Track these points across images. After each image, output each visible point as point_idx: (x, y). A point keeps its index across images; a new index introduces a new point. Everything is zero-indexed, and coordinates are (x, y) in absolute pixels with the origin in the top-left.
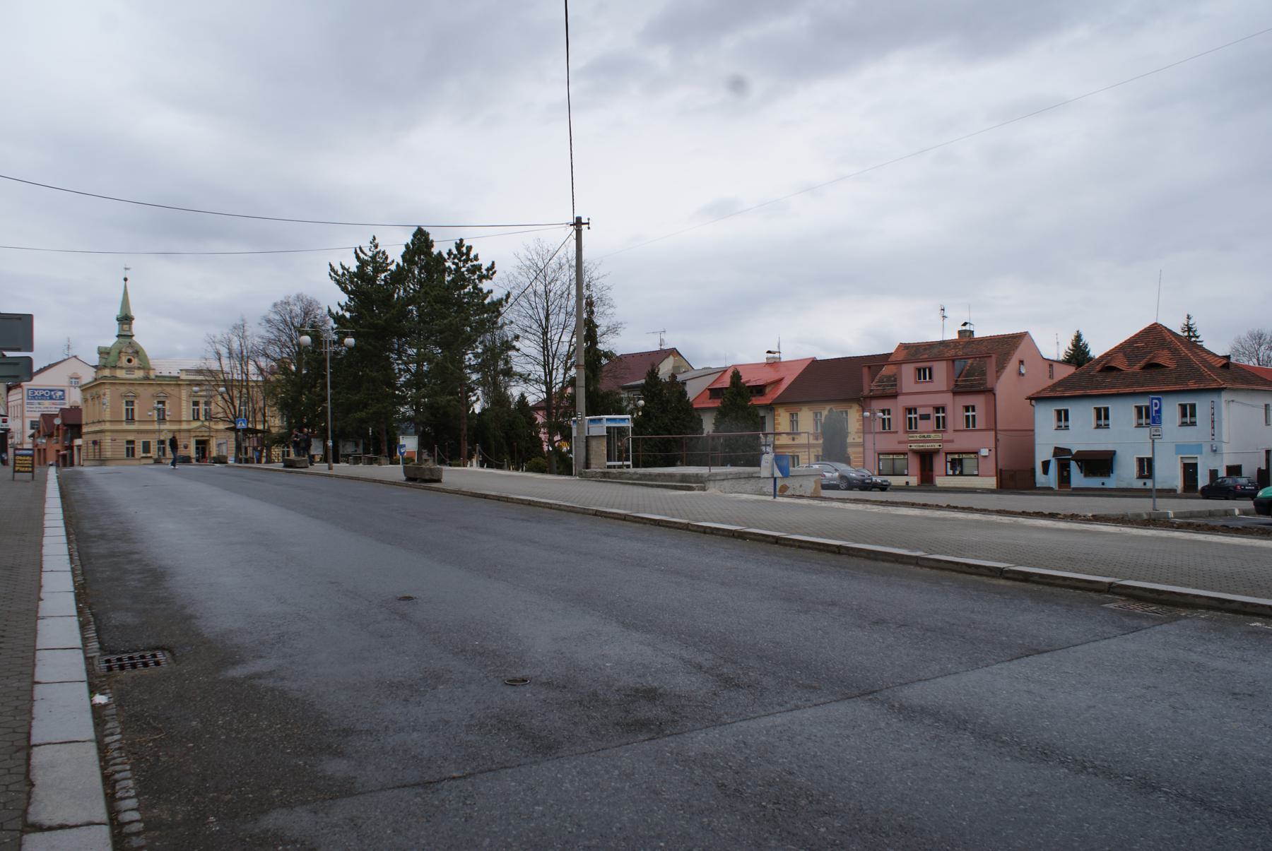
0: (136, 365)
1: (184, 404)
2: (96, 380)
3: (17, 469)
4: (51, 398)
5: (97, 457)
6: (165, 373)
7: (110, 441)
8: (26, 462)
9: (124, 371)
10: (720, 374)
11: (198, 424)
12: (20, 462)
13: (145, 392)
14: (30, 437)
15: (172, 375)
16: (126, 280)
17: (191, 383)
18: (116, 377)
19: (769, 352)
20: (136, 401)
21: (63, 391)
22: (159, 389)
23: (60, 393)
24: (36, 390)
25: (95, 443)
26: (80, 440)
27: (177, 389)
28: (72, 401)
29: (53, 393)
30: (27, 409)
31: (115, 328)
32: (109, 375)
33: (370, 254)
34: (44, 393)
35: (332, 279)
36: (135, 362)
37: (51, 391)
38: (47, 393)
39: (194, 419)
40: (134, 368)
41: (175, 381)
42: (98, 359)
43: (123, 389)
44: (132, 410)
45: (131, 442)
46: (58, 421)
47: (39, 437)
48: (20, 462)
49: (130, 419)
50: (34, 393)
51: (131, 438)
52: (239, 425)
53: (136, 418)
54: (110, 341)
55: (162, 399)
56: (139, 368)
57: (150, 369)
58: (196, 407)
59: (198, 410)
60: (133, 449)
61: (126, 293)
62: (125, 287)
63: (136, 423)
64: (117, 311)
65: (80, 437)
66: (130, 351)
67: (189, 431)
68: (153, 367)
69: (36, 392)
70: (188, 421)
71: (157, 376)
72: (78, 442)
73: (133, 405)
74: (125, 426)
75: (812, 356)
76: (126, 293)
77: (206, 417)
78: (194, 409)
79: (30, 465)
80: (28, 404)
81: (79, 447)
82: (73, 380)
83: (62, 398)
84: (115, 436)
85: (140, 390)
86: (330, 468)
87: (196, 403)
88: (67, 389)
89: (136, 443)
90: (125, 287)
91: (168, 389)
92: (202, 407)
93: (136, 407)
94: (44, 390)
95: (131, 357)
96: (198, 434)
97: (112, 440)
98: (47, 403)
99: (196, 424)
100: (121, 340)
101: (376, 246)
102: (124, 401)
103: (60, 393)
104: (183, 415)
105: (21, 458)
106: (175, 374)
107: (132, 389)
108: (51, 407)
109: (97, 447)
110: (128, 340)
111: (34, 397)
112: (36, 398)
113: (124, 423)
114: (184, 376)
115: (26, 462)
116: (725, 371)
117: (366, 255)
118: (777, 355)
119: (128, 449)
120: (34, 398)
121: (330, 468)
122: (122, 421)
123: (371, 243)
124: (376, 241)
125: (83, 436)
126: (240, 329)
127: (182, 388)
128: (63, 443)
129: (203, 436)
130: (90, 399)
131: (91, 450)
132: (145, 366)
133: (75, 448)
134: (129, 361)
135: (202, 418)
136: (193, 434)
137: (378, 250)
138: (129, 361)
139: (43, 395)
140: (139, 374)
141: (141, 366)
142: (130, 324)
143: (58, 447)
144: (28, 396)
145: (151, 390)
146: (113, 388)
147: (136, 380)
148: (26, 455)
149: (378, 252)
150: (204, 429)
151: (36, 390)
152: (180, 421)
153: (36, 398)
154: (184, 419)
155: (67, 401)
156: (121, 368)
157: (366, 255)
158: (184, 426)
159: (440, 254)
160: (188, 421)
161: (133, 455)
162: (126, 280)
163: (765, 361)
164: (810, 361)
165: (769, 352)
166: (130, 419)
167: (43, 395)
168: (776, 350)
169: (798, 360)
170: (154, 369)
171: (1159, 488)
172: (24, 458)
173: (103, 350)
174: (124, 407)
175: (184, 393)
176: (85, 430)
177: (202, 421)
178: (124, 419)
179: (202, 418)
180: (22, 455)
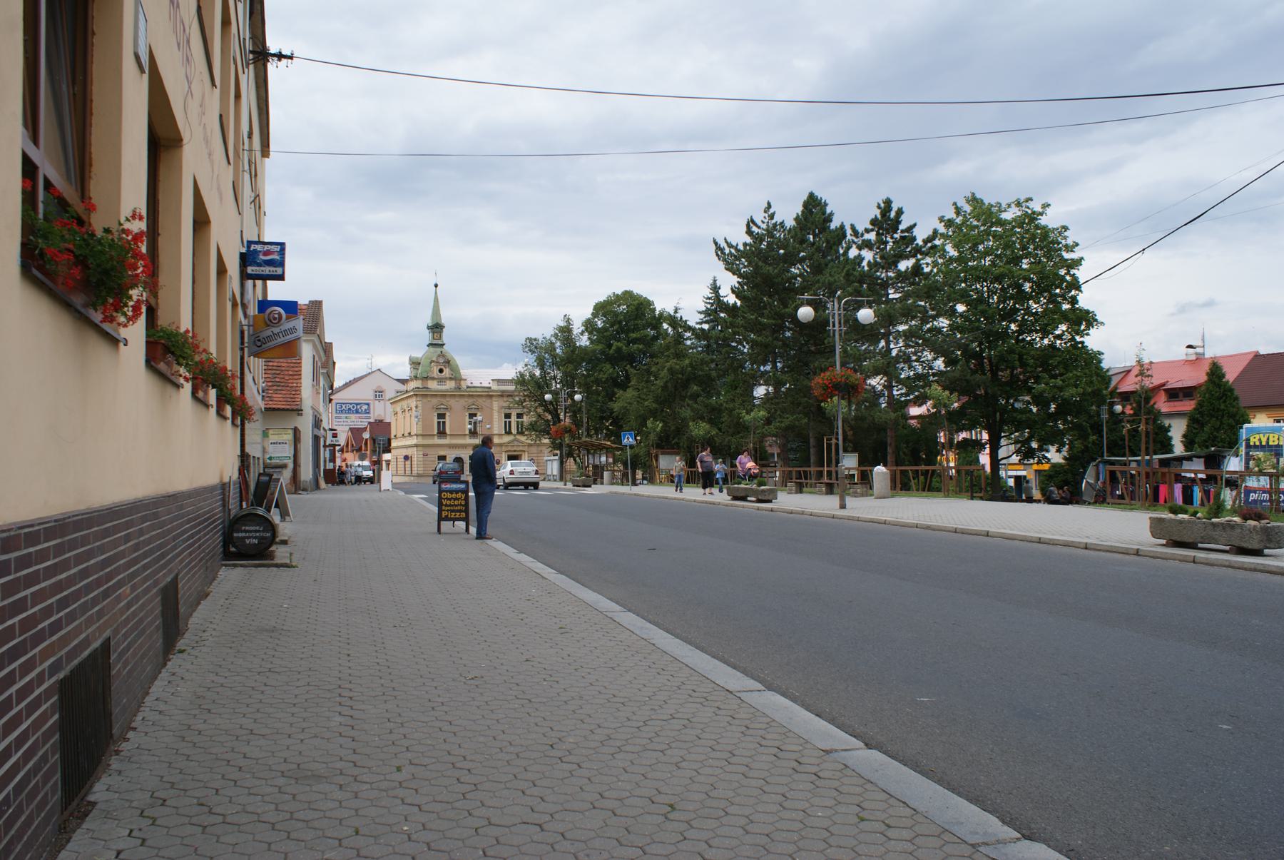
0: (447, 376)
1: (496, 415)
3: (444, 514)
4: (357, 412)
5: (408, 472)
6: (476, 384)
8: (456, 502)
10: (1124, 374)
11: (510, 438)
12: (448, 502)
13: (457, 404)
15: (484, 385)
16: (436, 286)
17: (503, 394)
19: (1190, 347)
20: (448, 414)
21: (368, 404)
22: (471, 400)
23: (366, 407)
25: (406, 458)
26: (390, 454)
28: (376, 414)
31: (426, 337)
33: (764, 226)
34: (351, 406)
35: (719, 259)
36: (447, 372)
37: (357, 404)
39: (506, 432)
40: (446, 379)
41: (488, 394)
42: (409, 370)
43: (435, 401)
44: (444, 423)
46: (366, 435)
47: (347, 452)
48: (448, 502)
49: (442, 433)
51: (442, 453)
52: (626, 440)
53: (448, 431)
54: (420, 352)
55: (442, 412)
56: (451, 379)
57: (461, 379)
58: (508, 420)
59: (510, 422)
61: (436, 299)
62: (436, 293)
63: (448, 437)
64: (428, 320)
65: (389, 451)
66: (441, 360)
68: (463, 377)
69: (344, 406)
70: (500, 435)
71: (468, 387)
72: (386, 456)
73: (444, 418)
74: (437, 441)
75: (1254, 349)
76: (436, 299)
77: (1260, 447)
78: (505, 422)
79: (444, 508)
80: (336, 418)
81: (388, 462)
83: (367, 412)
84: (428, 451)
85: (452, 402)
86: (843, 506)
87: (508, 416)
88: (372, 403)
90: (436, 293)
91: (481, 401)
92: (514, 419)
93: (447, 420)
95: (442, 367)
96: (509, 448)
98: (353, 417)
99: (507, 439)
100: (432, 349)
101: (772, 217)
102: (467, 414)
103: (366, 407)
105: (449, 495)
106: (485, 384)
107: (443, 400)
108: (360, 421)
109: (408, 463)
110: (438, 350)
113: (436, 437)
114: (495, 387)
115: (456, 502)
116: (1129, 371)
117: (759, 227)
118: (1199, 350)
120: (341, 412)
121: (843, 506)
122: (465, 435)
123: (765, 212)
124: (771, 211)
126: (565, 332)
127: (494, 399)
128: (371, 459)
130: (400, 412)
131: (401, 465)
132: (457, 378)
133: (384, 463)
134: (441, 371)
135: (514, 430)
136: (504, 449)
137: (773, 221)
138: (441, 371)
139: (350, 409)
140: (451, 385)
142: (441, 332)
145: (463, 402)
146: (425, 400)
148: (457, 492)
149: (775, 225)
150: (516, 443)
155: (372, 415)
156: (433, 379)
157: (759, 227)
159: (842, 227)
160: (500, 435)
162: (436, 286)
163: (1184, 358)
164: (1251, 356)
165: (1190, 347)
166: (442, 433)
167: (350, 409)
168: (1200, 344)
169: (1231, 356)
171: (1161, 488)
172: (454, 496)
173: (415, 360)
174: (436, 420)
175: (496, 404)
176: (394, 444)
177: (515, 435)
178: (436, 431)
179: (514, 430)
180: (451, 492)
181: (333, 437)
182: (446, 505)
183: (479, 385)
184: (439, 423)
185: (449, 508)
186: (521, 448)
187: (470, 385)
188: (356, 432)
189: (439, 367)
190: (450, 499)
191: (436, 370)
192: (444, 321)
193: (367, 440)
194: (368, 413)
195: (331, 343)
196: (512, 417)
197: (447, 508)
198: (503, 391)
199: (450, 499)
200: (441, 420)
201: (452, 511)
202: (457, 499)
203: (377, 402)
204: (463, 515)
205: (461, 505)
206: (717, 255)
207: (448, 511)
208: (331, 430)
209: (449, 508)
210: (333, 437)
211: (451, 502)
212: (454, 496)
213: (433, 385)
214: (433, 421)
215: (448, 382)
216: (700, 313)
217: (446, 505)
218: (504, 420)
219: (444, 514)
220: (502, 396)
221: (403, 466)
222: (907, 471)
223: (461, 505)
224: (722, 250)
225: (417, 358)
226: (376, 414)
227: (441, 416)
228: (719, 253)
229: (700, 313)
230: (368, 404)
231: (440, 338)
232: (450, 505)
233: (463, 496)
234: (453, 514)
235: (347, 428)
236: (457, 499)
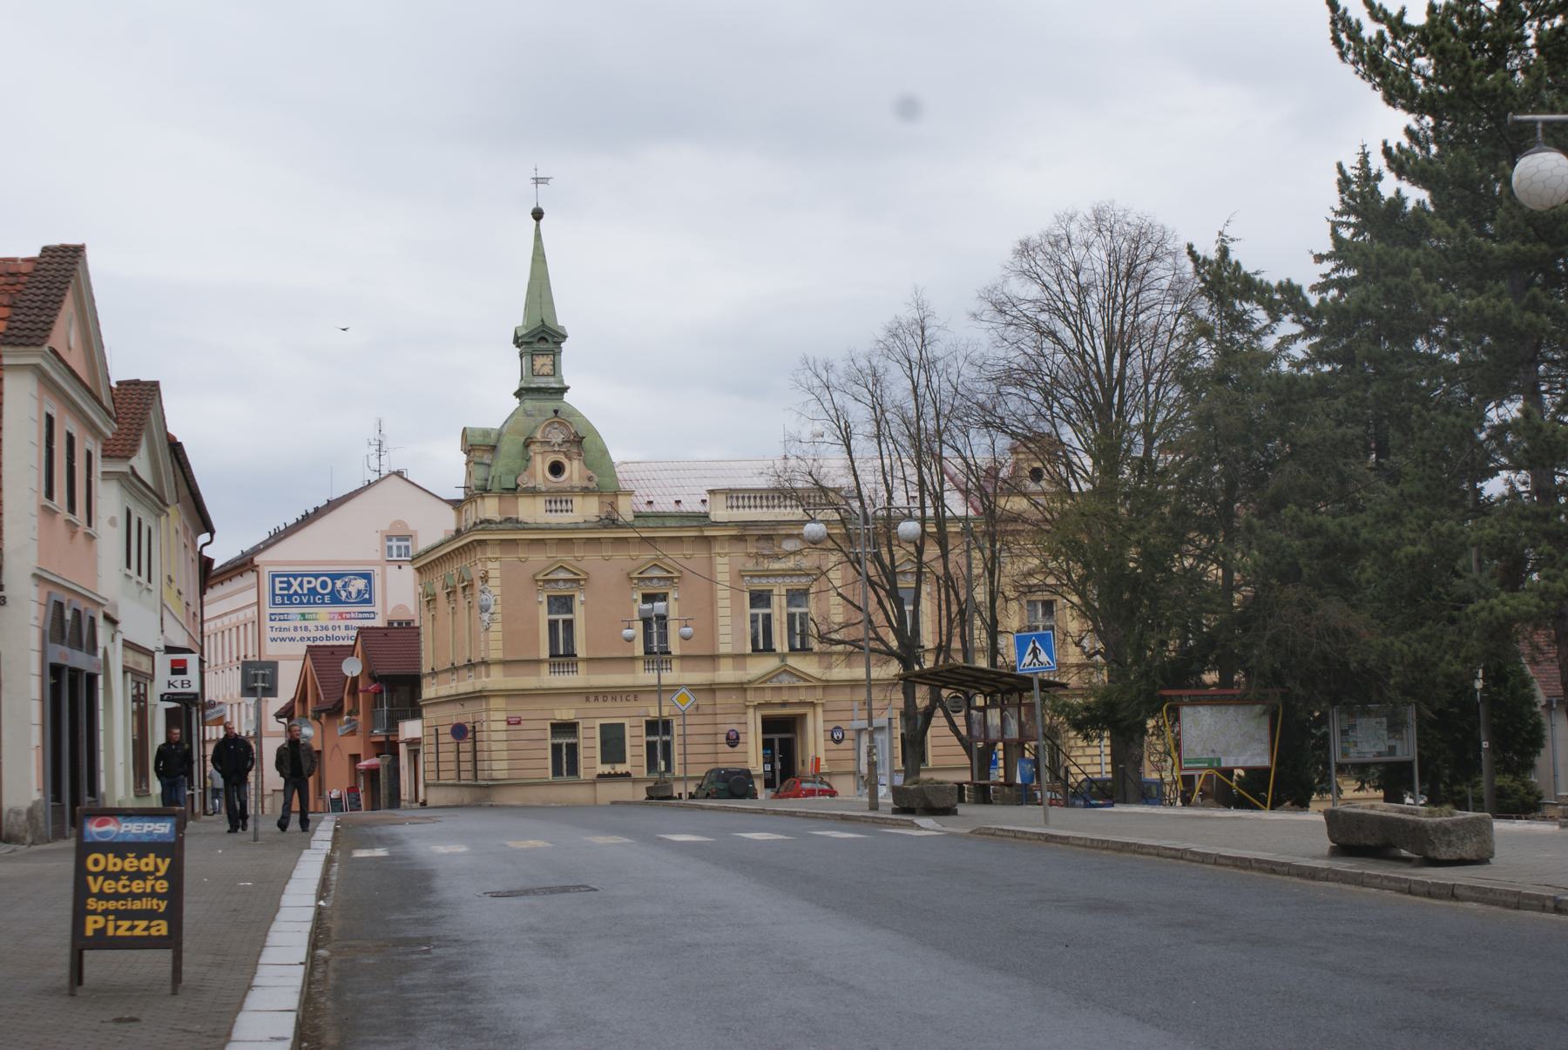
0: (577, 481)
1: (723, 596)
2: (458, 532)
3: (91, 925)
4: (335, 599)
6: (665, 505)
7: (503, 726)
8: (137, 887)
9: (540, 503)
11: (767, 664)
12: (110, 885)
14: (278, 716)
16: (538, 215)
17: (743, 533)
18: (517, 521)
20: (579, 597)
21: (367, 576)
22: (647, 555)
23: (360, 584)
24: (295, 577)
25: (459, 731)
27: (700, 554)
28: (391, 606)
29: (339, 584)
30: (268, 634)
31: (508, 369)
32: (497, 518)
34: (317, 583)
35: (1342, 55)
36: (574, 471)
37: (335, 577)
38: (324, 585)
39: (755, 649)
40: (571, 491)
43: (539, 559)
45: (565, 728)
46: (352, 667)
48: (110, 885)
49: (563, 656)
50: (290, 585)
51: (564, 714)
53: (581, 650)
55: (563, 590)
56: (586, 491)
58: (761, 611)
60: (573, 749)
62: (538, 236)
64: (515, 318)
65: (416, 714)
66: (557, 437)
67: (741, 687)
68: (624, 486)
70: (738, 657)
72: (410, 729)
74: (644, 676)
81: (414, 743)
82: (395, 543)
83: (365, 598)
84: (520, 709)
85: (590, 561)
87: (760, 598)
88: (377, 570)
89: (676, 729)
90: (538, 236)
92: (779, 610)
93: (579, 616)
94: (316, 576)
95: (561, 458)
97: (509, 723)
98: (323, 614)
99: (761, 667)
100: (530, 404)
102: (543, 598)
103: (360, 584)
104: (722, 639)
105: (112, 863)
106: (692, 505)
107: (565, 557)
109: (466, 746)
110: (550, 405)
111: (290, 597)
112: (296, 599)
113: (545, 668)
114: (720, 512)
115: (137, 887)
119: (556, 749)
120: (289, 599)
125: (425, 712)
129: (784, 704)
130: (441, 595)
132: (604, 485)
133: (403, 749)
134: (556, 469)
136: (753, 698)
138: (556, 469)
139: (313, 591)
140: (586, 509)
141: (592, 485)
142: (555, 353)
143: (355, 745)
144: (274, 595)
146: (510, 558)
147: (575, 528)
148: (141, 848)
150: (786, 681)
151: (295, 577)
152: (714, 658)
153: (296, 599)
154: (724, 649)
155: (378, 607)
156: (534, 492)
158: (727, 673)
160: (738, 657)
161: (573, 769)
162: (538, 215)
166: (563, 656)
167: (313, 591)
170: (630, 493)
172: (130, 863)
173: (478, 440)
174: (544, 617)
175: (725, 564)
176: (429, 691)
177: (783, 657)
179: (780, 643)
181: (174, 672)
182: (102, 896)
183: (672, 508)
184: (553, 625)
185: (112, 905)
186: (803, 696)
187: (645, 509)
188: (323, 657)
189: (551, 458)
190: (115, 876)
191: (541, 465)
192: (564, 317)
193: (355, 680)
194: (369, 601)
195: (155, 386)
196: (775, 600)
197: (102, 905)
198: (745, 525)
199: (115, 876)
200: (561, 617)
201: (121, 915)
202: (139, 875)
203: (392, 569)
204: (161, 928)
205: (153, 894)
206: (1336, 41)
207: (105, 913)
208: (170, 650)
209: (112, 905)
210: (174, 672)
211: (120, 886)
212: (130, 863)
213: (531, 510)
214: (535, 620)
215: (577, 501)
216: (1319, 258)
217: (102, 896)
218: (749, 611)
219: (91, 925)
220: (740, 539)
221: (452, 756)
222: (773, 740)
223: (153, 894)
224: (1354, 31)
225: (486, 433)
226: (391, 606)
227: (562, 603)
228: (1343, 37)
229: (1319, 258)
230: (367, 576)
231: (555, 370)
232: (116, 896)
233: (163, 867)
234: (126, 924)
235: (301, 649)
236: (139, 875)
